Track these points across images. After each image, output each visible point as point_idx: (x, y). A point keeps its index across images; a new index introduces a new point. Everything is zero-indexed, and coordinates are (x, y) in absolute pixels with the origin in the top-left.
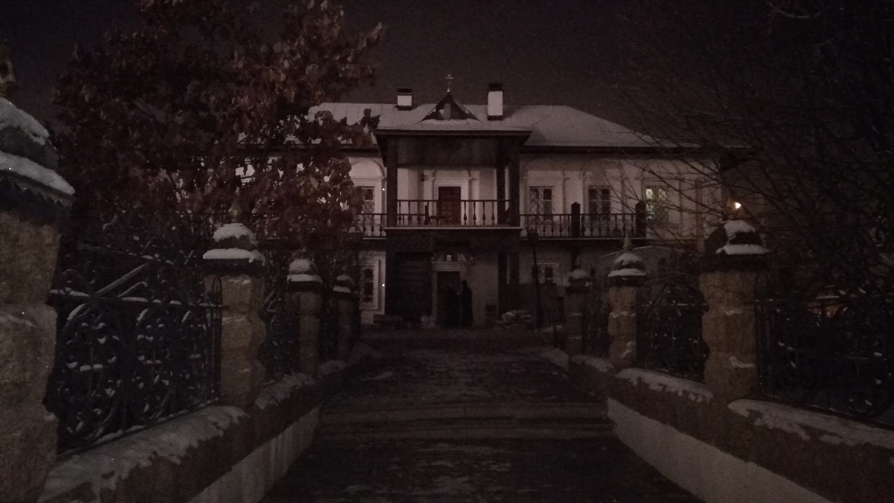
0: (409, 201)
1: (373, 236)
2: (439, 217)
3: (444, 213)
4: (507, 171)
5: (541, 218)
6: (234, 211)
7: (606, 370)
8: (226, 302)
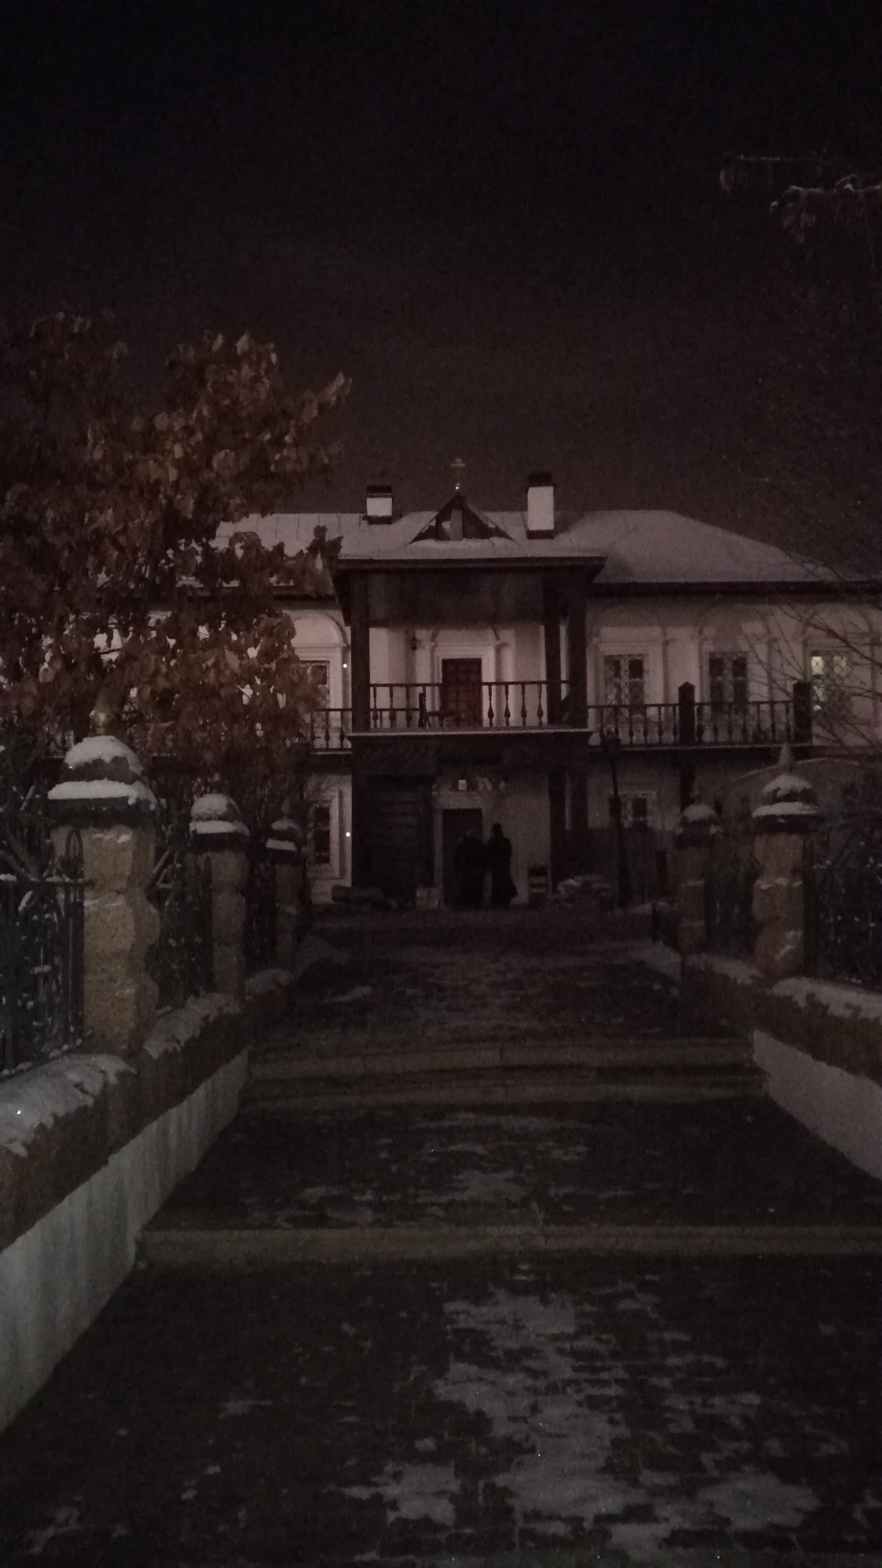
0: (391, 686)
1: (327, 749)
2: (444, 713)
3: (452, 706)
4: (563, 630)
5: (626, 712)
6: (100, 716)
7: (749, 982)
8: (88, 875)
